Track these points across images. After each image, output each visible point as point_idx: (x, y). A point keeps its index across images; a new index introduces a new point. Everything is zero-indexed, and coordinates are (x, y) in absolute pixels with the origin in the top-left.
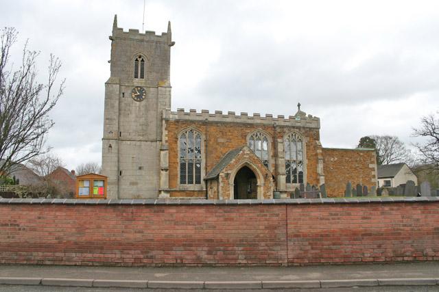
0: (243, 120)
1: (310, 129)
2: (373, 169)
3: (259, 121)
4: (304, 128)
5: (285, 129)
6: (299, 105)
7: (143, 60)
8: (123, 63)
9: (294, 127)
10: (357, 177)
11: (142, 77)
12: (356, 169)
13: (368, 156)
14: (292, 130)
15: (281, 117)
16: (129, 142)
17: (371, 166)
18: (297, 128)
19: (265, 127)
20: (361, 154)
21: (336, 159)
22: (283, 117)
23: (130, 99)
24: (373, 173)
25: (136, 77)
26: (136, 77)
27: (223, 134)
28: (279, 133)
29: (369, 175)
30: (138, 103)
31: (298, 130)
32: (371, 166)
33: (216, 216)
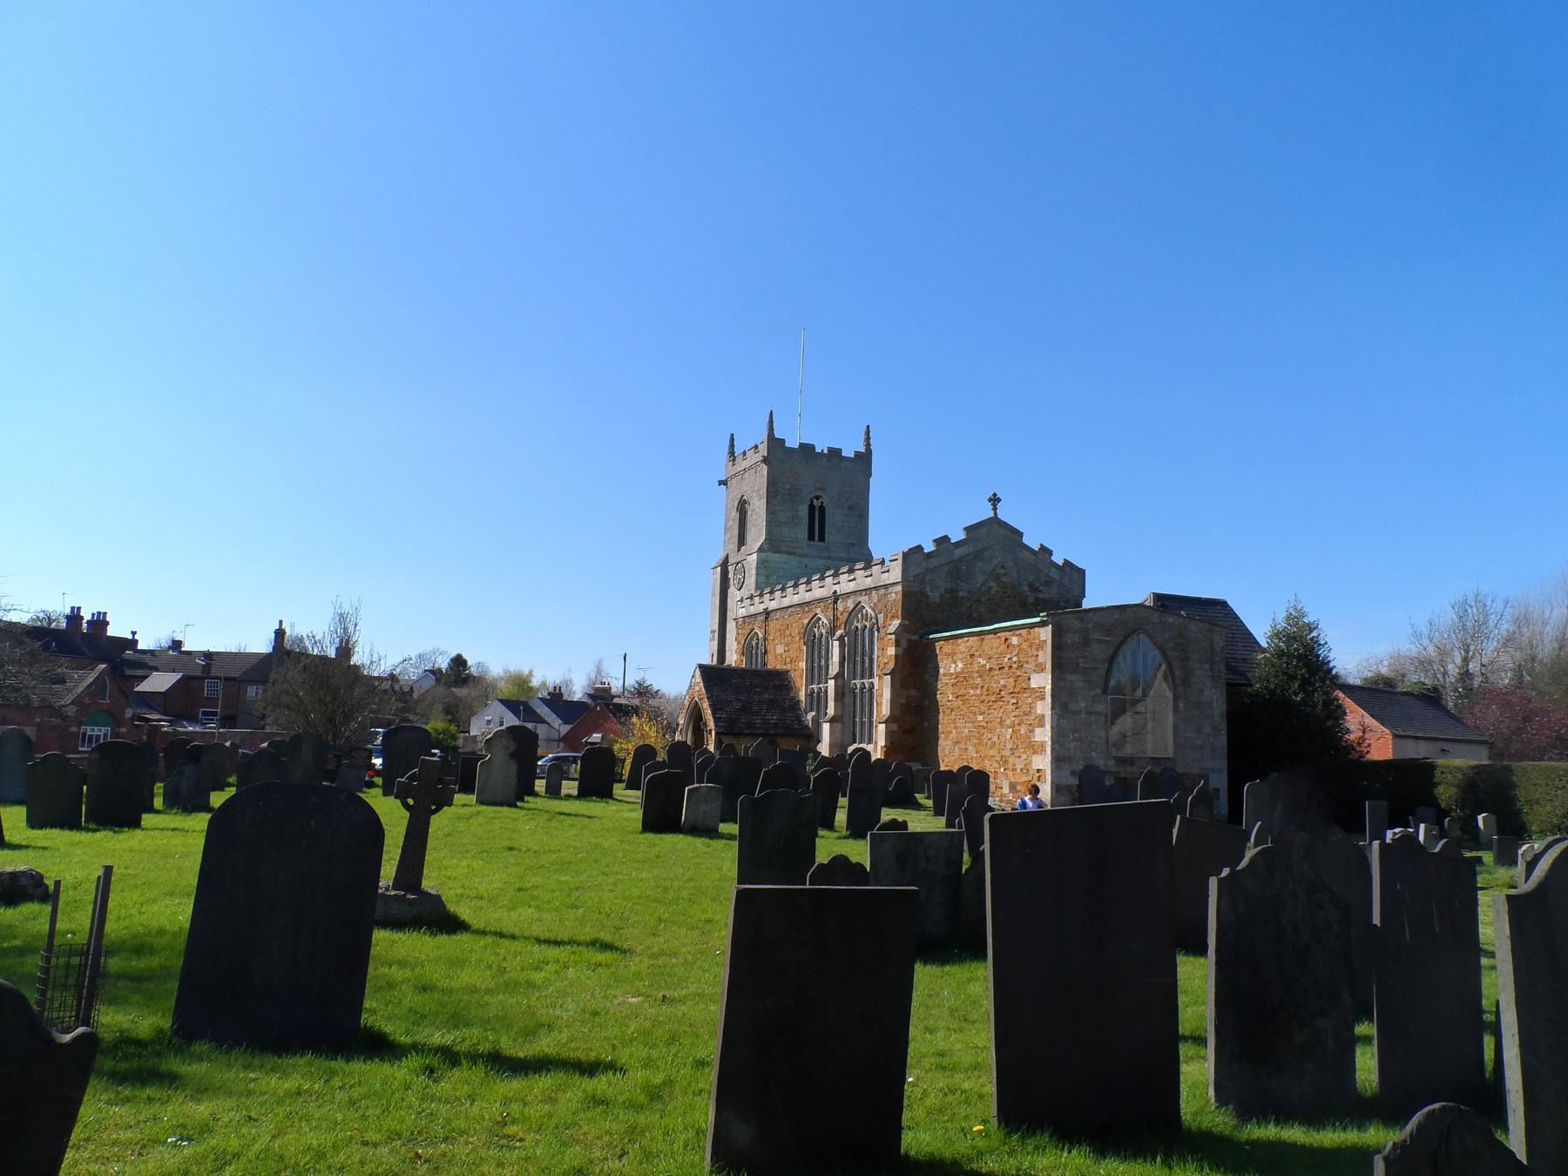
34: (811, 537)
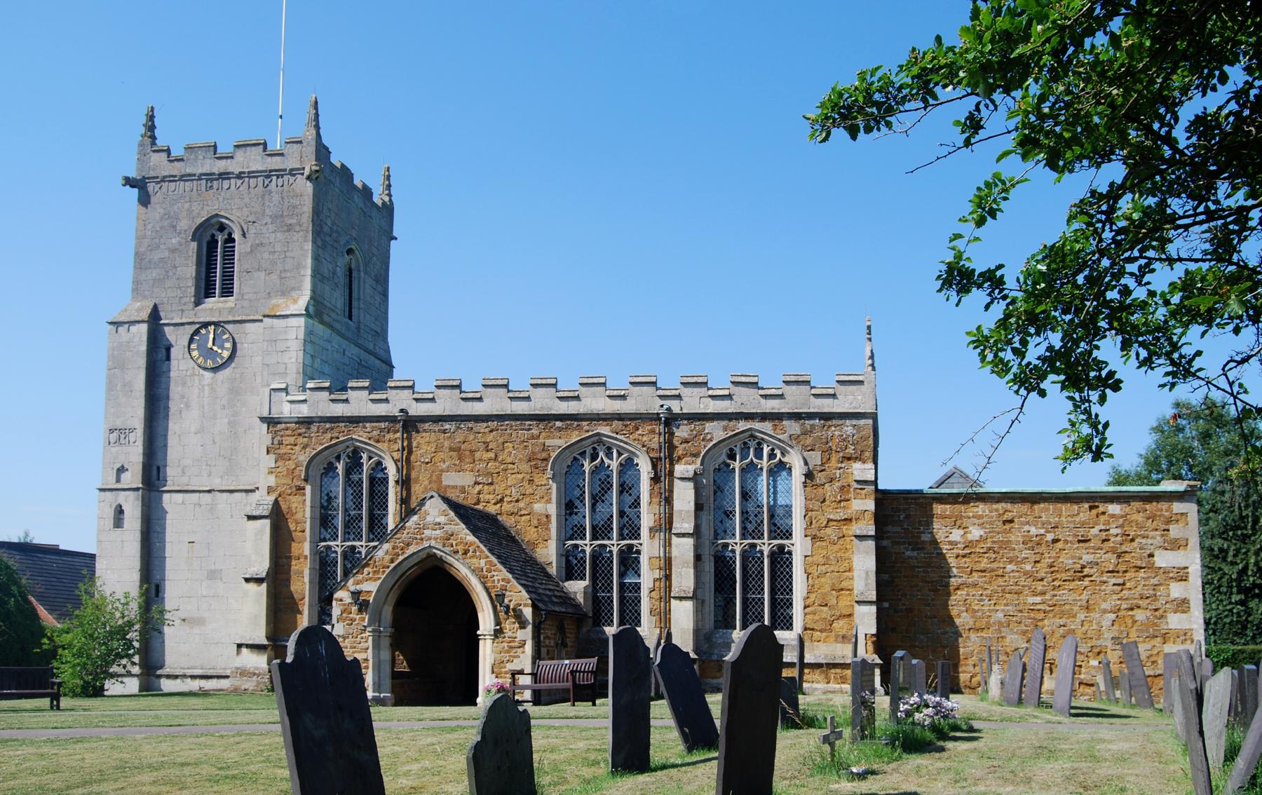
11: (227, 291)
17: (1164, 559)
21: (975, 533)
24: (1176, 590)
26: (209, 293)
30: (208, 375)
32: (1164, 559)
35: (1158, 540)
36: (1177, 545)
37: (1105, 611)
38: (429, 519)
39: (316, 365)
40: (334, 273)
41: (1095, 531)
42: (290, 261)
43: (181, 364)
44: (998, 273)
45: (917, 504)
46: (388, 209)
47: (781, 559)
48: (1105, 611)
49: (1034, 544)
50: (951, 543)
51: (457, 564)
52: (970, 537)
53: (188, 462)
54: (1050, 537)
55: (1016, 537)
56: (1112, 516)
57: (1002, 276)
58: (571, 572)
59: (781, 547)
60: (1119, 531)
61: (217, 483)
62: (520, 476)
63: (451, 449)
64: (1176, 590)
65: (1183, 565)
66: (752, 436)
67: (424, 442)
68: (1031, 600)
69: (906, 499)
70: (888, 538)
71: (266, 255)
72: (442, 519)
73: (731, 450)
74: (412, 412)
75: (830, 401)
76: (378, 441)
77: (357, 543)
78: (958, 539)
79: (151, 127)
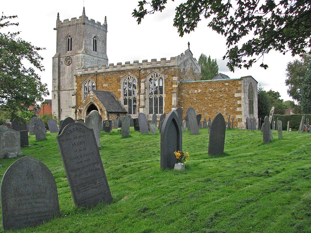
0: (119, 68)
1: (169, 67)
2: (240, 99)
3: (129, 68)
4: (163, 67)
5: (148, 71)
6: (44, 49)
7: (71, 39)
8: (61, 43)
9: (154, 68)
10: (221, 107)
11: (71, 50)
12: (219, 99)
13: (234, 85)
14: (153, 70)
15: (145, 61)
16: (64, 92)
17: (236, 95)
18: (157, 68)
19: (132, 71)
20: (227, 84)
21: (200, 91)
22: (121, 64)
23: (64, 65)
24: (239, 102)
25: (94, 50)
26: (68, 50)
27: (106, 80)
28: (143, 74)
29: (234, 104)
30: (68, 66)
31: (158, 70)
32: (236, 95)
33: (296, 139)
34: (94, 50)
35: (235, 91)
36: (239, 92)
37: (224, 107)
38: (91, 95)
39: (86, 63)
40: (90, 43)
41: (223, 89)
42: (80, 42)
43: (63, 66)
44: (264, 13)
45: (188, 85)
46: (106, 26)
47: (161, 99)
48: (224, 107)
49: (211, 93)
50: (195, 93)
51: (95, 104)
52: (198, 92)
53: (65, 85)
54: (214, 91)
55: (207, 91)
56: (226, 85)
57: (263, 12)
58: (125, 103)
59: (161, 96)
60: (228, 89)
61: (70, 88)
62: (115, 84)
63: (104, 79)
64: (239, 102)
65: (240, 96)
66: (155, 72)
67: (100, 78)
68: (210, 105)
69: (187, 84)
70: (183, 93)
71: (76, 41)
72: (92, 95)
73: (152, 75)
74: (98, 72)
75: (169, 63)
76: (92, 78)
77: (126, 97)
78: (196, 92)
79: (58, 17)
